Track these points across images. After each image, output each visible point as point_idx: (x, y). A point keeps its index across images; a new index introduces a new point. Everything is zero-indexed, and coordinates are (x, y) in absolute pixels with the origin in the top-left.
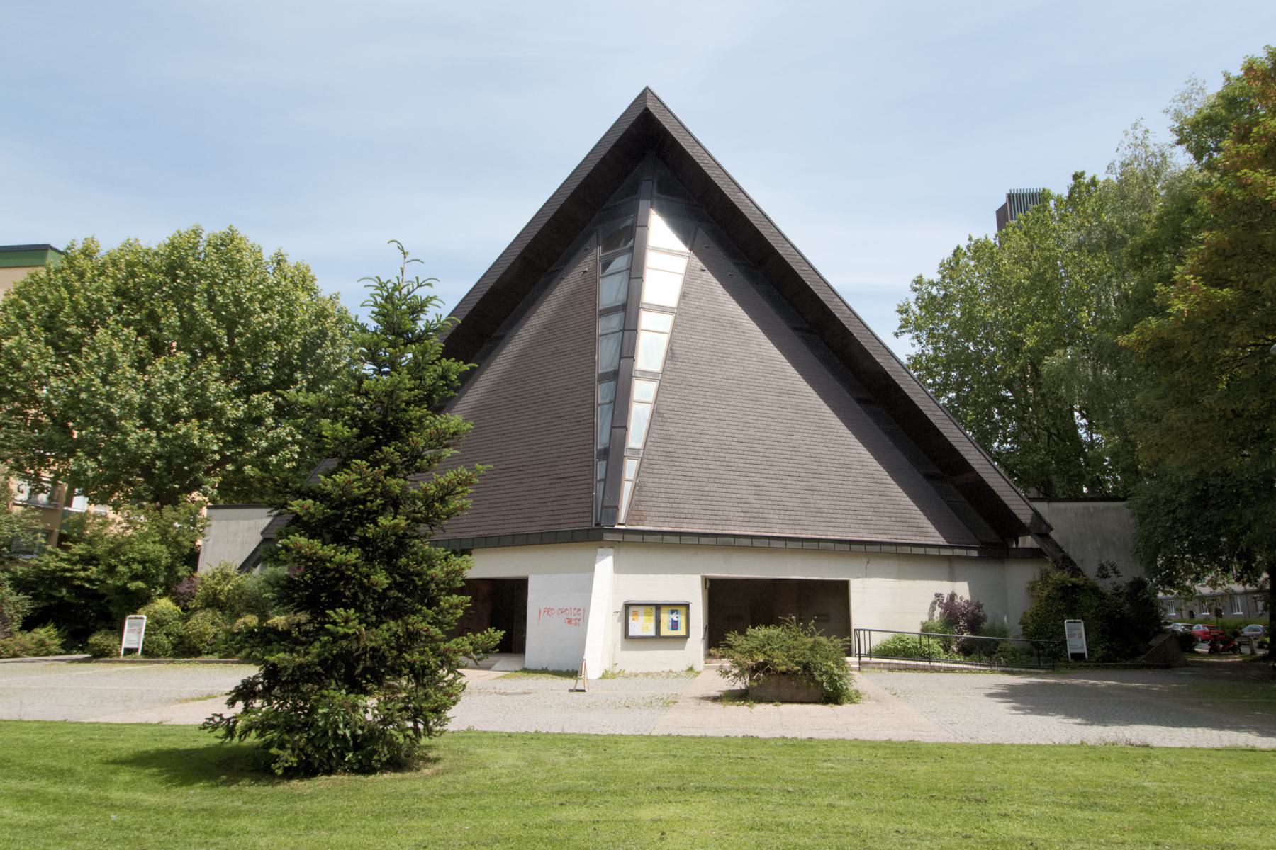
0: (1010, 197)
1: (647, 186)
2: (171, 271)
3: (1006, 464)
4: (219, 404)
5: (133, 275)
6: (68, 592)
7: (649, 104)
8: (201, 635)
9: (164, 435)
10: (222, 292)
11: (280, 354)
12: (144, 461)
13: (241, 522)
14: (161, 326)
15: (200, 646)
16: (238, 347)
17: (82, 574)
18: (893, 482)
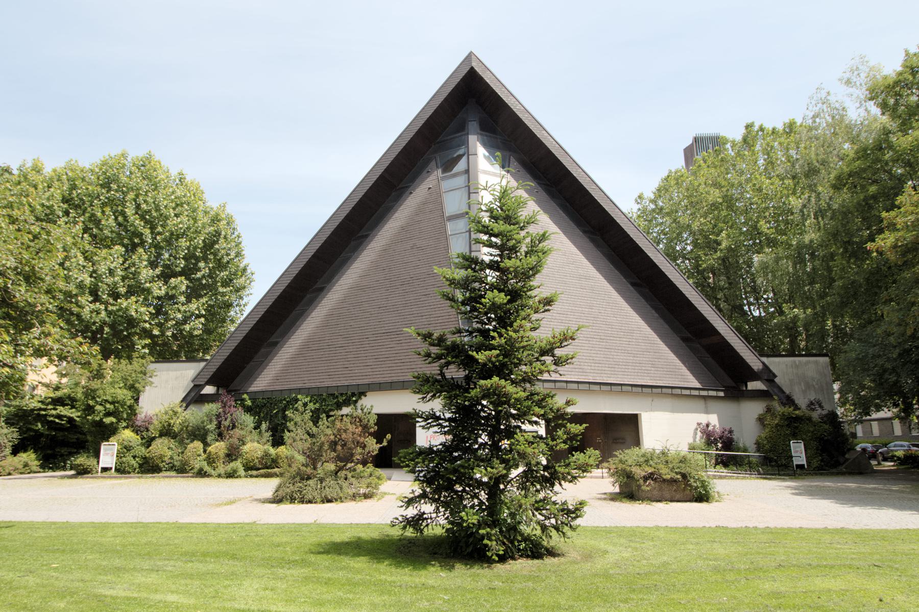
0: (696, 139)
1: (473, 125)
2: (106, 185)
4: (148, 285)
5: (74, 187)
6: (42, 426)
7: (474, 64)
8: (161, 457)
9: (110, 308)
10: (145, 201)
11: (188, 248)
12: (94, 328)
13: (170, 372)
14: (101, 226)
15: (161, 465)
16: (159, 243)
17: (54, 412)
18: (662, 343)
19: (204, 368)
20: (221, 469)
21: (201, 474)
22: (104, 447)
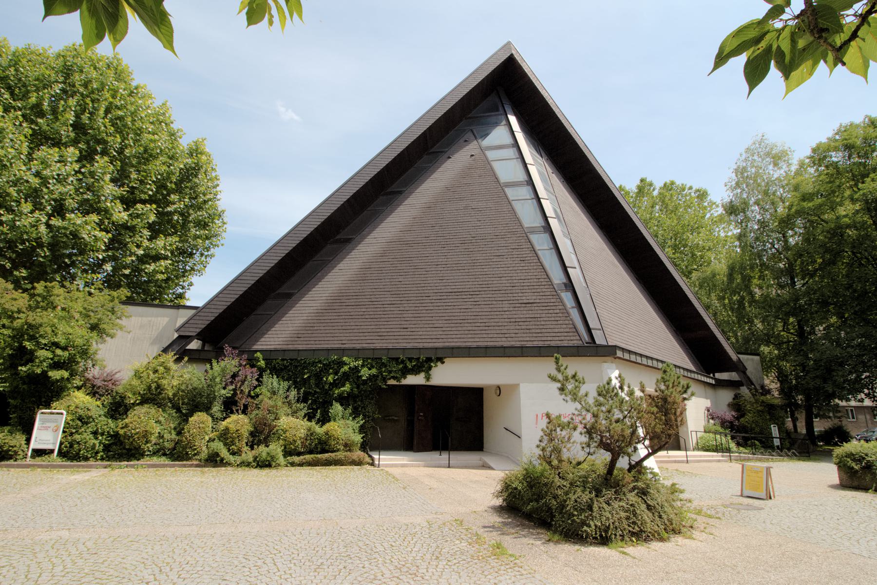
3: (732, 345)
7: (514, 52)
19: (191, 319)
20: (248, 455)
21: (214, 460)
22: (41, 418)
